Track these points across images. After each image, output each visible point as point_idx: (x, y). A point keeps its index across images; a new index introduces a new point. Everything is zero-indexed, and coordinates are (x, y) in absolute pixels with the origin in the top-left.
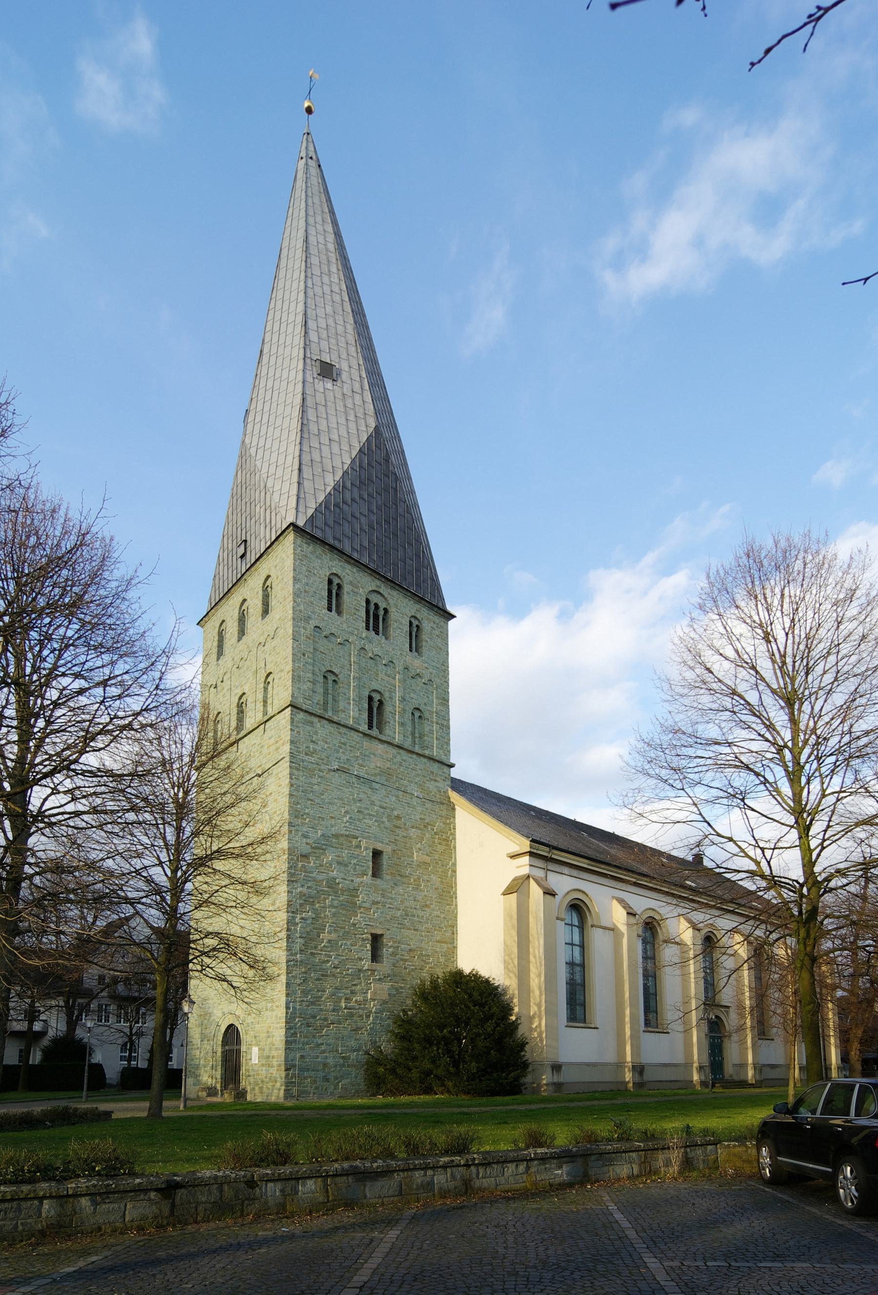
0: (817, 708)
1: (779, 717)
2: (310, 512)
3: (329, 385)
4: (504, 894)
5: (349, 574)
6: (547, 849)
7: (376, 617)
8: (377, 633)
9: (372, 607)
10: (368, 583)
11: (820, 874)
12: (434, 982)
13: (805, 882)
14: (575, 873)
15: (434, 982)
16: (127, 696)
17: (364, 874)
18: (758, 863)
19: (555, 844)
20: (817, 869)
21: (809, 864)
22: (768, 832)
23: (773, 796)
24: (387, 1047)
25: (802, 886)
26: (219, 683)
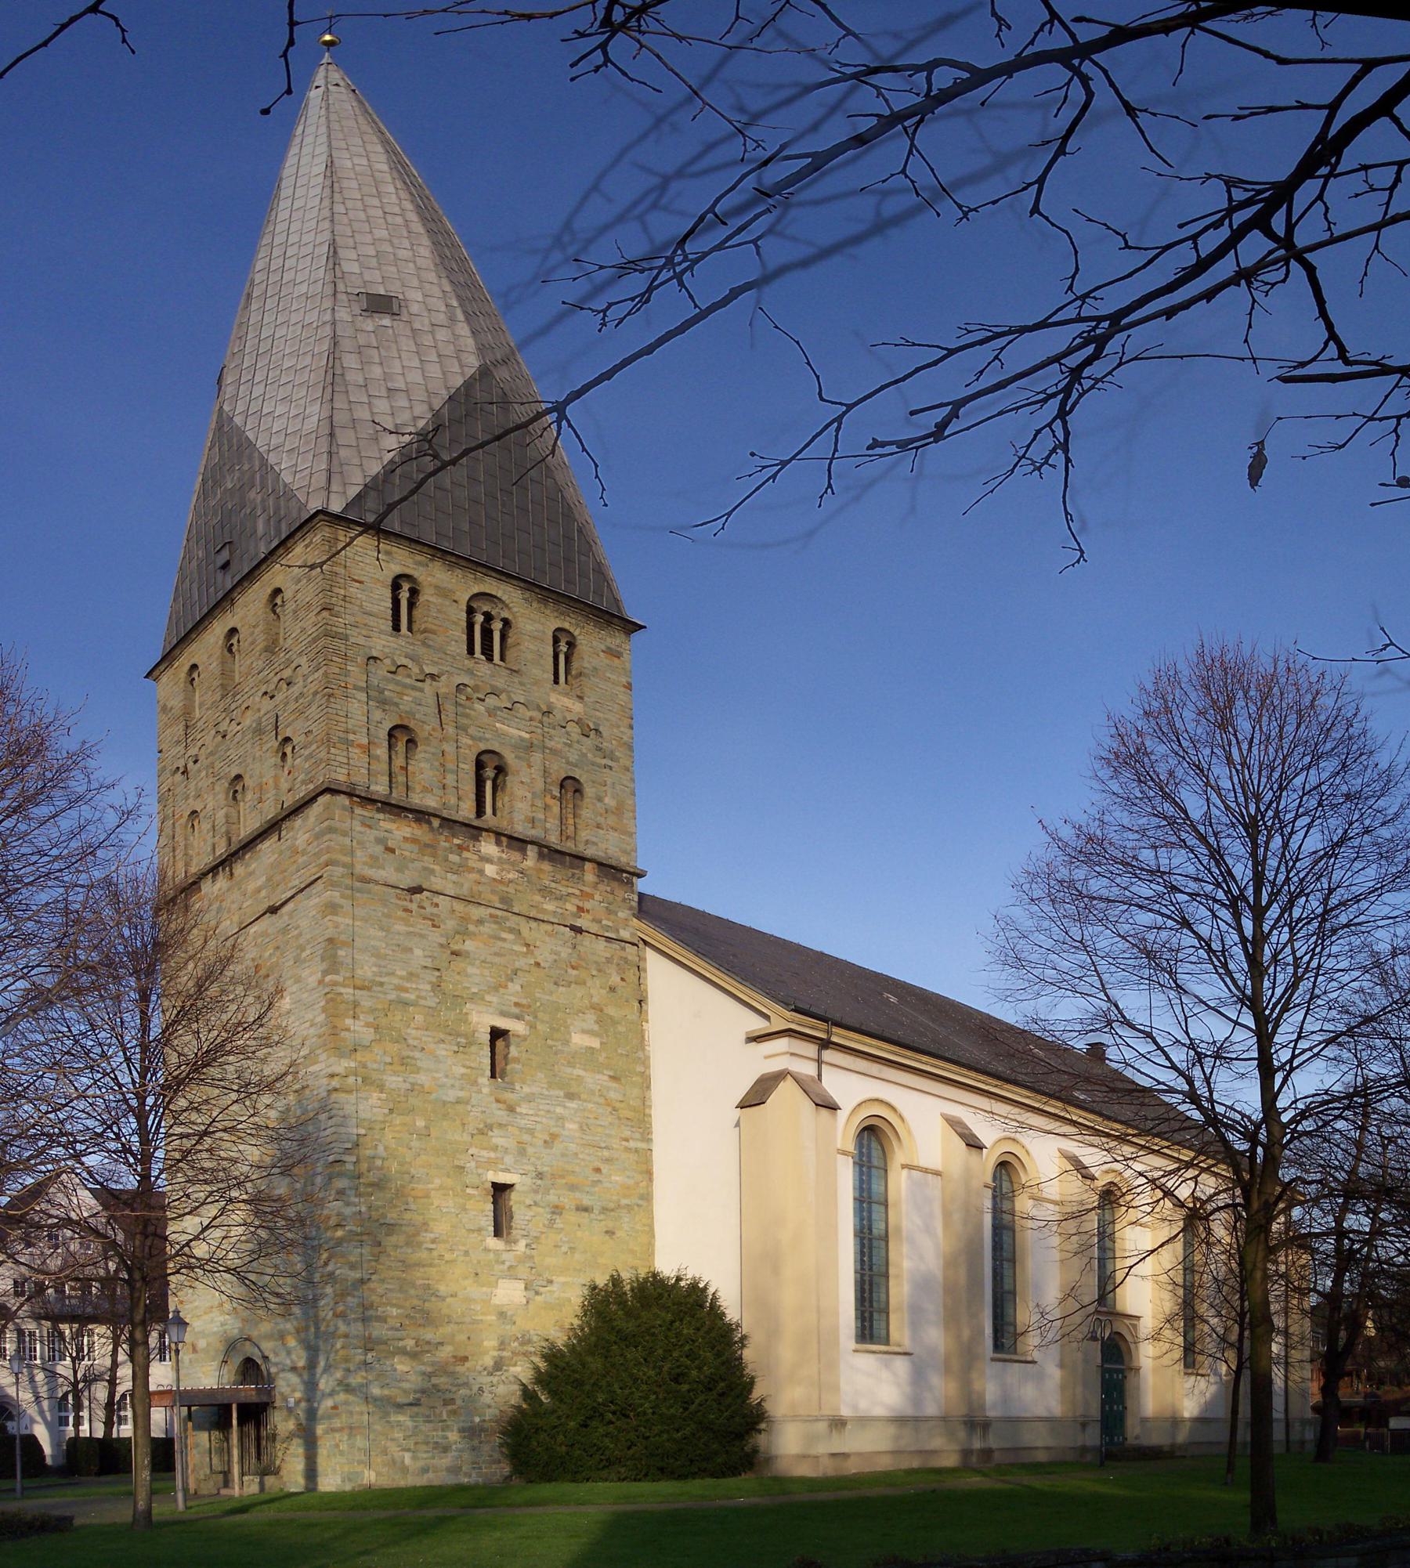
0: (1294, 845)
1: (1235, 848)
2: (353, 491)
3: (386, 321)
4: (742, 1106)
5: (434, 576)
6: (824, 1026)
7: (487, 633)
8: (490, 658)
9: (479, 618)
10: (464, 586)
11: (1285, 1110)
12: (616, 1281)
13: (1263, 1120)
14: (875, 1068)
15: (616, 1281)
16: (175, 1085)
17: (483, 1075)
18: (1190, 1081)
19: (837, 1017)
20: (1281, 1103)
21: (1269, 1097)
22: (1210, 1029)
23: (1220, 975)
24: (543, 1365)
25: (1258, 1127)
26: (190, 765)
